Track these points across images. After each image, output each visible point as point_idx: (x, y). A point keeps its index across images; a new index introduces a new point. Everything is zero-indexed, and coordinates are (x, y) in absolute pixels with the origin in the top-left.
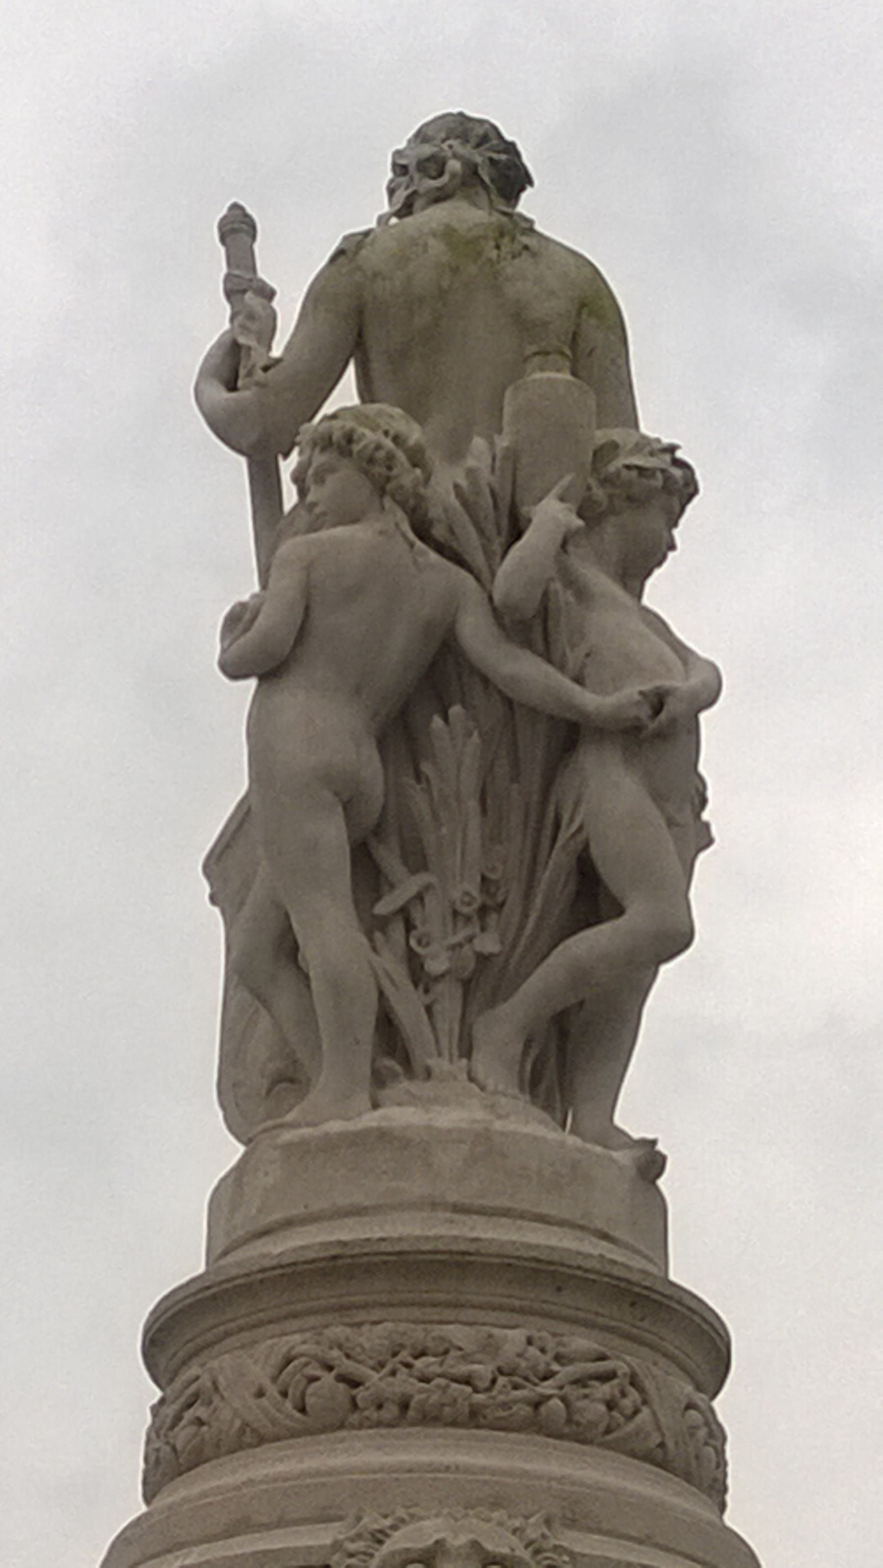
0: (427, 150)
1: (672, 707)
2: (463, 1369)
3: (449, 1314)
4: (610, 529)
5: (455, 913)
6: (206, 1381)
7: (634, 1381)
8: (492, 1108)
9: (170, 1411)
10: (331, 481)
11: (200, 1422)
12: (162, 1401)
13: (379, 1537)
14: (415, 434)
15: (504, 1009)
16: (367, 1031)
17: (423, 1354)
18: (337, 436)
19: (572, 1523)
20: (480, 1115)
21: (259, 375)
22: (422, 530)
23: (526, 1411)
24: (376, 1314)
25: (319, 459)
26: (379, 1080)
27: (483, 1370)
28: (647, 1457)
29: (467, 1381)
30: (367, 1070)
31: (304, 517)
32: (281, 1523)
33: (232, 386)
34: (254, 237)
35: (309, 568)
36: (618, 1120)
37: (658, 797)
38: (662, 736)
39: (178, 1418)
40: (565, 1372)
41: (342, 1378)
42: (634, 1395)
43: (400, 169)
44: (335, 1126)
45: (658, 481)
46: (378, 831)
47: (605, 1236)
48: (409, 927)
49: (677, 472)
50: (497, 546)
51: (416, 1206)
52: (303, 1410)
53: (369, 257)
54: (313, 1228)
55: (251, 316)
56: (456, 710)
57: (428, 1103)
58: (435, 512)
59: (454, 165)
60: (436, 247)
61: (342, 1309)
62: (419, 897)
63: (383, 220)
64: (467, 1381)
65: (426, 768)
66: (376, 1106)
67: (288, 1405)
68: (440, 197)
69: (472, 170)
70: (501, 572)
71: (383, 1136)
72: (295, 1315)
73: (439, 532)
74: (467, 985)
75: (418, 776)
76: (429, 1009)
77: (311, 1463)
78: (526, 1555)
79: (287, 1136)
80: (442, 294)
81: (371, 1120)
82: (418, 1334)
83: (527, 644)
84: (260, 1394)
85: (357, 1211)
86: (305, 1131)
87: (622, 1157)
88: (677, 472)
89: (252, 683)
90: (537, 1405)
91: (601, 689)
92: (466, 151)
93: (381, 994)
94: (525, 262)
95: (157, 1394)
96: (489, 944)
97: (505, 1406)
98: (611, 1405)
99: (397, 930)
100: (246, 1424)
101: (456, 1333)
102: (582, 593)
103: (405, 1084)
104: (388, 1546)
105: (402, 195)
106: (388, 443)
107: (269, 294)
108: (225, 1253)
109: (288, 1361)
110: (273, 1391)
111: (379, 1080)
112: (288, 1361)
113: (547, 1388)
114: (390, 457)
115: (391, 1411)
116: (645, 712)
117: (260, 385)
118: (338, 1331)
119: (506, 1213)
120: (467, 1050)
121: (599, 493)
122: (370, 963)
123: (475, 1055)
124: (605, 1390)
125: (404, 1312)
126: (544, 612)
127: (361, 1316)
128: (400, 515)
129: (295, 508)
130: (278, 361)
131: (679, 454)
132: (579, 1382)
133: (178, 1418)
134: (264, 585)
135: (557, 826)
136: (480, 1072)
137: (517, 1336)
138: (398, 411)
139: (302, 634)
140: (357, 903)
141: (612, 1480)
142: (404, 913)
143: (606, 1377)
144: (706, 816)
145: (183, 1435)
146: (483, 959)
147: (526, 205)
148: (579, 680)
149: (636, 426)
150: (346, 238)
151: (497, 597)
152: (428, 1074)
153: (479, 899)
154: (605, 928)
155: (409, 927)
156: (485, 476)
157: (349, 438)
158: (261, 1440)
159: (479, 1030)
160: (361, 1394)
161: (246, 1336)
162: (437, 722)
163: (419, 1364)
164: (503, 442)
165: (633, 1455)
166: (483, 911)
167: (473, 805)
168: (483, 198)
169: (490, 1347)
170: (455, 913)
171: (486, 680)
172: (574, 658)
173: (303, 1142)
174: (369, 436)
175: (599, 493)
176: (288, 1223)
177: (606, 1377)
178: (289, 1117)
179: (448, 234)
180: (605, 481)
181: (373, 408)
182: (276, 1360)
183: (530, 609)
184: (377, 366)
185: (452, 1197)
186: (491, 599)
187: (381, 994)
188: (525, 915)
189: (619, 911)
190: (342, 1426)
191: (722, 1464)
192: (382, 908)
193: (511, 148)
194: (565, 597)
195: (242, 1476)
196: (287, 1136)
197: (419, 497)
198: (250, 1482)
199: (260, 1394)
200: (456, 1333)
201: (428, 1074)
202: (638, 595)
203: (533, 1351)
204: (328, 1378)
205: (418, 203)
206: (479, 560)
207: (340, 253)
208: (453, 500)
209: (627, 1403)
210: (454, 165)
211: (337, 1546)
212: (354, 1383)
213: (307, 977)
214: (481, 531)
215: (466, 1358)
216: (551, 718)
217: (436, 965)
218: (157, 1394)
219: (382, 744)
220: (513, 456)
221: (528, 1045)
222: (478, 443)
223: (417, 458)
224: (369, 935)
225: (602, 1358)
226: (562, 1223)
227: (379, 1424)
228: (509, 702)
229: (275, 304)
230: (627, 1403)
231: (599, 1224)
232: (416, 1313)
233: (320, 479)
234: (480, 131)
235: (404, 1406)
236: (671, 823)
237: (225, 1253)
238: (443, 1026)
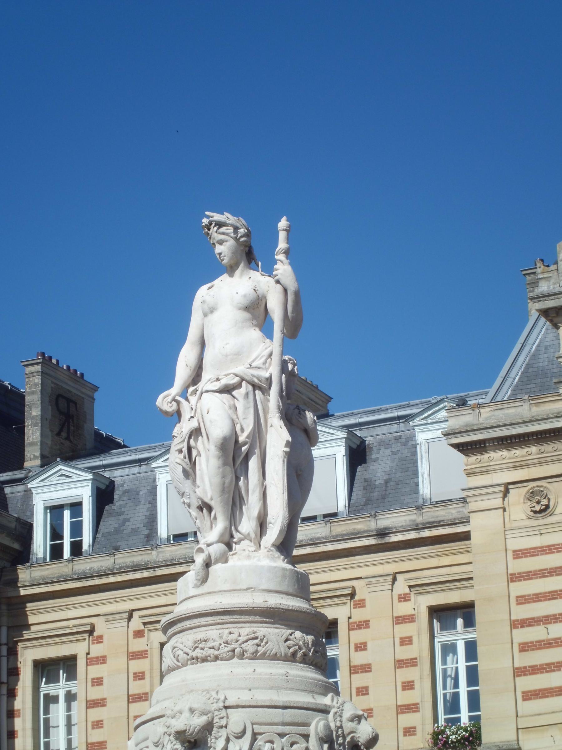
29: (213, 648)
64: (213, 648)
100: (169, 666)
177: (256, 638)
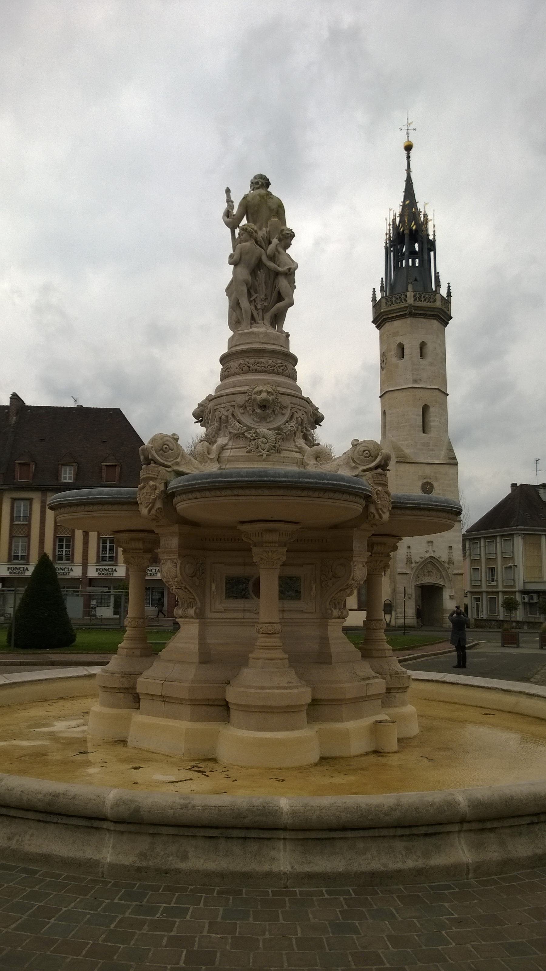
0: (256, 180)
1: (292, 270)
2: (264, 365)
3: (261, 358)
4: (283, 243)
5: (261, 300)
6: (229, 366)
7: (286, 366)
8: (267, 328)
9: (224, 370)
10: (244, 235)
11: (228, 371)
12: (223, 368)
13: (254, 389)
14: (256, 228)
15: (268, 314)
16: (250, 317)
17: (258, 363)
18: (245, 229)
19: (278, 386)
20: (266, 330)
21: (232, 217)
22: (256, 242)
23: (272, 371)
24: (252, 358)
25: (242, 232)
26: (251, 324)
27: (266, 365)
28: (287, 376)
29: (264, 367)
30: (250, 323)
31: (239, 240)
32: (240, 386)
33: (228, 217)
34: (230, 192)
35: (241, 249)
36: (283, 329)
37: (289, 283)
38: (290, 274)
39: (225, 371)
40: (277, 365)
41: (248, 366)
42: (286, 368)
43: (252, 183)
44: (246, 331)
45: (289, 235)
46: (250, 288)
47: (282, 346)
48: (255, 302)
49: (292, 234)
50: (267, 245)
51: (257, 342)
52: (242, 370)
53: (249, 199)
54: (243, 345)
55: (230, 206)
56: (262, 270)
57: (258, 327)
58: (258, 240)
59: (260, 183)
60: (258, 197)
61: (247, 357)
62: (257, 297)
63: (250, 192)
64: (264, 367)
65: (257, 278)
66: (251, 328)
67: (241, 370)
68: (258, 188)
69: (262, 183)
70: (268, 250)
71: (252, 333)
72: (241, 358)
73: (259, 243)
74: (263, 310)
75: (256, 279)
76: (258, 313)
77: (244, 378)
78: (272, 391)
79: (240, 332)
80: (259, 205)
81: (250, 330)
82: (257, 361)
83: (272, 261)
84: (237, 368)
85: (249, 343)
86: (242, 331)
87: (284, 335)
88: (292, 234)
89: (233, 266)
90: (273, 370)
91: (282, 268)
92: (262, 181)
93: (252, 312)
94: (271, 200)
95: (222, 367)
96: (266, 304)
97: (269, 370)
98: (283, 370)
99: (253, 302)
101: (263, 360)
102: (279, 252)
103: (255, 325)
104: (255, 390)
105: (252, 187)
106: (252, 230)
107: (232, 202)
108: (231, 348)
109: (241, 364)
110: (238, 368)
111: (251, 324)
112: (241, 364)
113: (275, 368)
114: (252, 233)
115: (254, 371)
116: (287, 271)
117: (233, 218)
118: (247, 360)
119: (269, 343)
120: (263, 320)
121: (281, 237)
122: (442, 577)
123: (265, 320)
124: (282, 368)
125: (256, 357)
126: (274, 256)
127: (250, 358)
128: (254, 240)
129: (238, 238)
130: (235, 215)
131: (292, 231)
132: (279, 367)
133: (225, 371)
134: (234, 250)
135: (275, 287)
136: (265, 323)
137: (270, 361)
138: (253, 224)
139: (240, 259)
140: (248, 298)
141: (283, 380)
142: (254, 300)
143: (282, 366)
144: (295, 284)
145: (226, 373)
146: (265, 306)
147: (270, 189)
148: (279, 266)
149: (286, 226)
150: (245, 195)
151: (267, 254)
152: (258, 323)
153: (265, 298)
154: (282, 303)
155: (255, 302)
156: (266, 235)
157: (246, 229)
158: (237, 374)
159: (265, 317)
160: (250, 369)
161: (234, 360)
162: (259, 272)
163: (258, 365)
164: (268, 229)
165: (285, 376)
166: (265, 299)
167: (264, 284)
168: (264, 189)
169: (267, 362)
170: (261, 300)
171: (265, 265)
172: (278, 263)
173: (241, 333)
174: (249, 229)
175: (281, 237)
176: (240, 345)
177: (282, 366)
178: (239, 329)
179: (259, 195)
180: (282, 235)
181: (250, 224)
182: (239, 363)
183: (273, 255)
184: (250, 216)
185: (262, 341)
186: (266, 253)
187: (252, 312)
188: (271, 299)
189: (284, 300)
190: (248, 373)
191: (296, 376)
192: (251, 299)
193: (268, 180)
194: (277, 253)
195: (235, 379)
196: (240, 332)
197: (256, 238)
198: (236, 380)
199: (237, 368)
200: (263, 360)
201: (258, 323)
202: (285, 251)
203: (273, 363)
204: (246, 366)
205: (255, 189)
206: (264, 247)
207: (244, 198)
208: (261, 239)
209: (285, 369)
210: (260, 183)
211: (248, 390)
212: (249, 367)
213: (241, 309)
214: (265, 243)
215: (264, 364)
216: (275, 272)
217: (259, 307)
218: (222, 367)
219: (251, 274)
220: (269, 231)
221: (271, 318)
222: (264, 229)
223: (256, 232)
224: (250, 303)
225: (282, 363)
226: (276, 345)
227: (253, 373)
228: (269, 269)
229: (234, 204)
230: (285, 369)
231: (281, 345)
232: (257, 358)
233: (242, 235)
234: (263, 177)
235: (256, 370)
236: (291, 287)
237: (231, 348)
238: (260, 316)
